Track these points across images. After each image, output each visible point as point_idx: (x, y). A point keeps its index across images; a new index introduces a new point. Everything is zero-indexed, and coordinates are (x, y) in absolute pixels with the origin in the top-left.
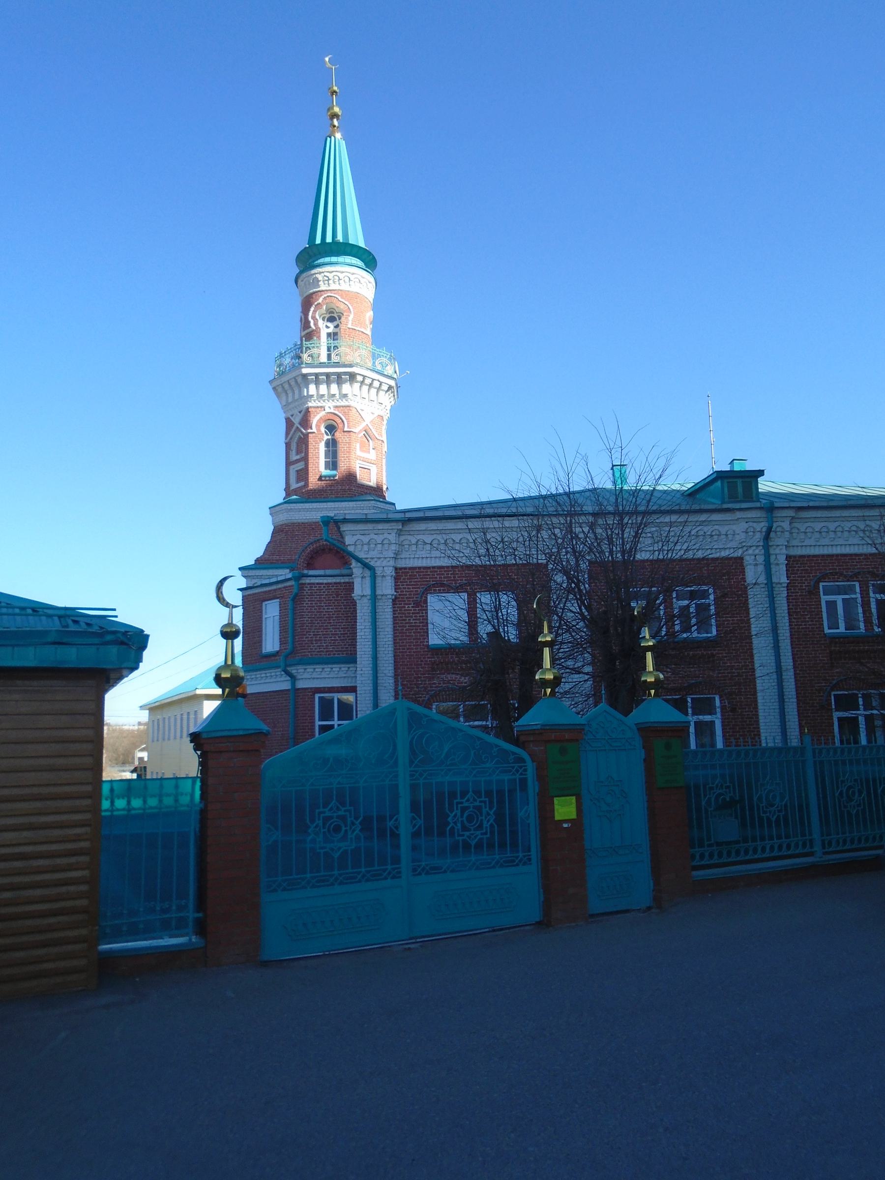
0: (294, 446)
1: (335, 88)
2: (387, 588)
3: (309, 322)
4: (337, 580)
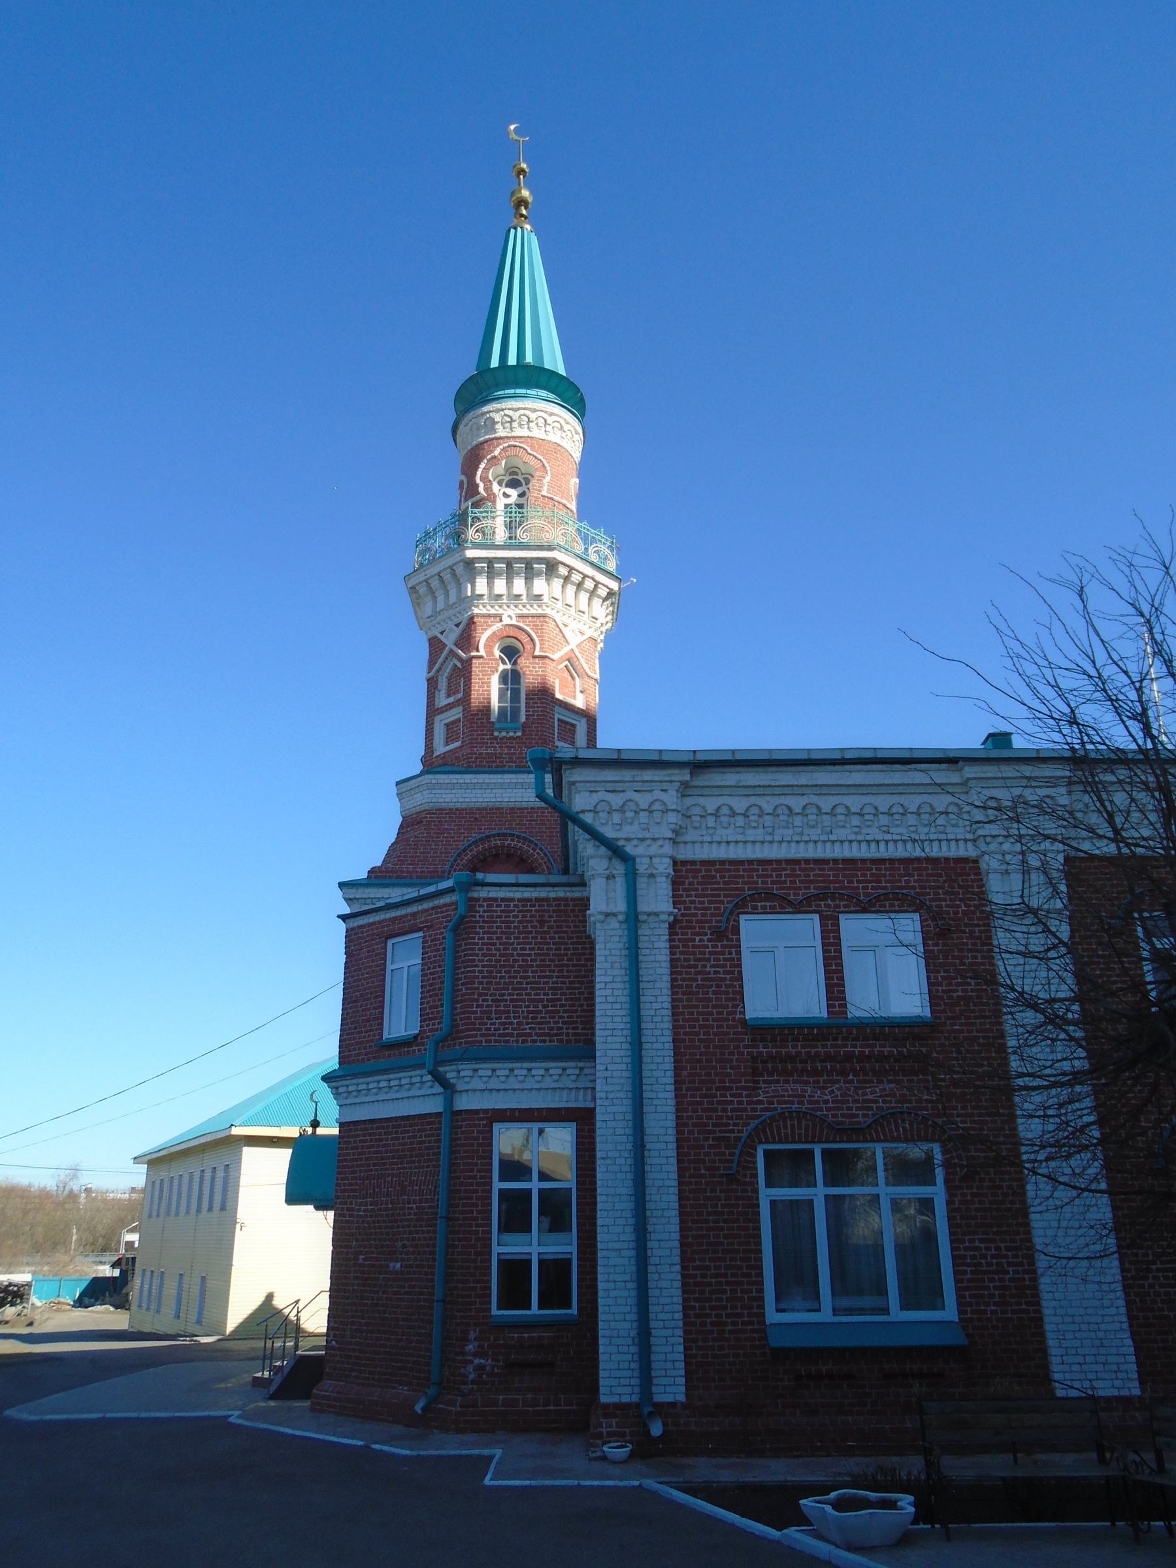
0: (443, 684)
1: (524, 166)
2: (658, 899)
3: (477, 486)
4: (542, 893)
